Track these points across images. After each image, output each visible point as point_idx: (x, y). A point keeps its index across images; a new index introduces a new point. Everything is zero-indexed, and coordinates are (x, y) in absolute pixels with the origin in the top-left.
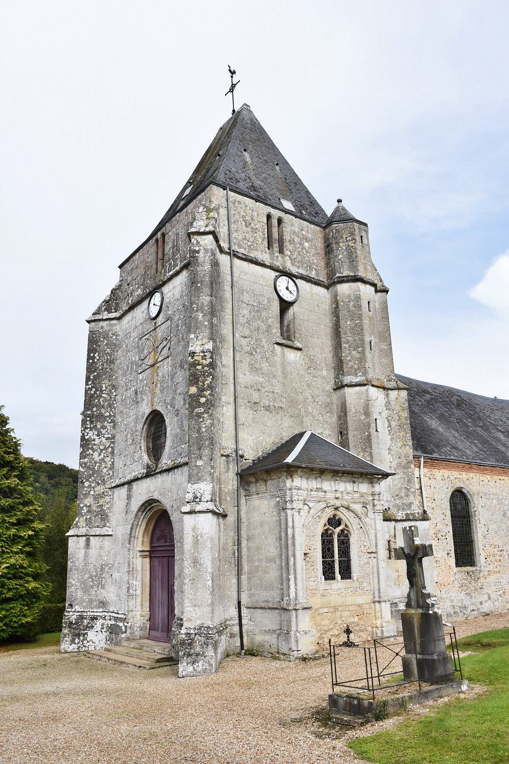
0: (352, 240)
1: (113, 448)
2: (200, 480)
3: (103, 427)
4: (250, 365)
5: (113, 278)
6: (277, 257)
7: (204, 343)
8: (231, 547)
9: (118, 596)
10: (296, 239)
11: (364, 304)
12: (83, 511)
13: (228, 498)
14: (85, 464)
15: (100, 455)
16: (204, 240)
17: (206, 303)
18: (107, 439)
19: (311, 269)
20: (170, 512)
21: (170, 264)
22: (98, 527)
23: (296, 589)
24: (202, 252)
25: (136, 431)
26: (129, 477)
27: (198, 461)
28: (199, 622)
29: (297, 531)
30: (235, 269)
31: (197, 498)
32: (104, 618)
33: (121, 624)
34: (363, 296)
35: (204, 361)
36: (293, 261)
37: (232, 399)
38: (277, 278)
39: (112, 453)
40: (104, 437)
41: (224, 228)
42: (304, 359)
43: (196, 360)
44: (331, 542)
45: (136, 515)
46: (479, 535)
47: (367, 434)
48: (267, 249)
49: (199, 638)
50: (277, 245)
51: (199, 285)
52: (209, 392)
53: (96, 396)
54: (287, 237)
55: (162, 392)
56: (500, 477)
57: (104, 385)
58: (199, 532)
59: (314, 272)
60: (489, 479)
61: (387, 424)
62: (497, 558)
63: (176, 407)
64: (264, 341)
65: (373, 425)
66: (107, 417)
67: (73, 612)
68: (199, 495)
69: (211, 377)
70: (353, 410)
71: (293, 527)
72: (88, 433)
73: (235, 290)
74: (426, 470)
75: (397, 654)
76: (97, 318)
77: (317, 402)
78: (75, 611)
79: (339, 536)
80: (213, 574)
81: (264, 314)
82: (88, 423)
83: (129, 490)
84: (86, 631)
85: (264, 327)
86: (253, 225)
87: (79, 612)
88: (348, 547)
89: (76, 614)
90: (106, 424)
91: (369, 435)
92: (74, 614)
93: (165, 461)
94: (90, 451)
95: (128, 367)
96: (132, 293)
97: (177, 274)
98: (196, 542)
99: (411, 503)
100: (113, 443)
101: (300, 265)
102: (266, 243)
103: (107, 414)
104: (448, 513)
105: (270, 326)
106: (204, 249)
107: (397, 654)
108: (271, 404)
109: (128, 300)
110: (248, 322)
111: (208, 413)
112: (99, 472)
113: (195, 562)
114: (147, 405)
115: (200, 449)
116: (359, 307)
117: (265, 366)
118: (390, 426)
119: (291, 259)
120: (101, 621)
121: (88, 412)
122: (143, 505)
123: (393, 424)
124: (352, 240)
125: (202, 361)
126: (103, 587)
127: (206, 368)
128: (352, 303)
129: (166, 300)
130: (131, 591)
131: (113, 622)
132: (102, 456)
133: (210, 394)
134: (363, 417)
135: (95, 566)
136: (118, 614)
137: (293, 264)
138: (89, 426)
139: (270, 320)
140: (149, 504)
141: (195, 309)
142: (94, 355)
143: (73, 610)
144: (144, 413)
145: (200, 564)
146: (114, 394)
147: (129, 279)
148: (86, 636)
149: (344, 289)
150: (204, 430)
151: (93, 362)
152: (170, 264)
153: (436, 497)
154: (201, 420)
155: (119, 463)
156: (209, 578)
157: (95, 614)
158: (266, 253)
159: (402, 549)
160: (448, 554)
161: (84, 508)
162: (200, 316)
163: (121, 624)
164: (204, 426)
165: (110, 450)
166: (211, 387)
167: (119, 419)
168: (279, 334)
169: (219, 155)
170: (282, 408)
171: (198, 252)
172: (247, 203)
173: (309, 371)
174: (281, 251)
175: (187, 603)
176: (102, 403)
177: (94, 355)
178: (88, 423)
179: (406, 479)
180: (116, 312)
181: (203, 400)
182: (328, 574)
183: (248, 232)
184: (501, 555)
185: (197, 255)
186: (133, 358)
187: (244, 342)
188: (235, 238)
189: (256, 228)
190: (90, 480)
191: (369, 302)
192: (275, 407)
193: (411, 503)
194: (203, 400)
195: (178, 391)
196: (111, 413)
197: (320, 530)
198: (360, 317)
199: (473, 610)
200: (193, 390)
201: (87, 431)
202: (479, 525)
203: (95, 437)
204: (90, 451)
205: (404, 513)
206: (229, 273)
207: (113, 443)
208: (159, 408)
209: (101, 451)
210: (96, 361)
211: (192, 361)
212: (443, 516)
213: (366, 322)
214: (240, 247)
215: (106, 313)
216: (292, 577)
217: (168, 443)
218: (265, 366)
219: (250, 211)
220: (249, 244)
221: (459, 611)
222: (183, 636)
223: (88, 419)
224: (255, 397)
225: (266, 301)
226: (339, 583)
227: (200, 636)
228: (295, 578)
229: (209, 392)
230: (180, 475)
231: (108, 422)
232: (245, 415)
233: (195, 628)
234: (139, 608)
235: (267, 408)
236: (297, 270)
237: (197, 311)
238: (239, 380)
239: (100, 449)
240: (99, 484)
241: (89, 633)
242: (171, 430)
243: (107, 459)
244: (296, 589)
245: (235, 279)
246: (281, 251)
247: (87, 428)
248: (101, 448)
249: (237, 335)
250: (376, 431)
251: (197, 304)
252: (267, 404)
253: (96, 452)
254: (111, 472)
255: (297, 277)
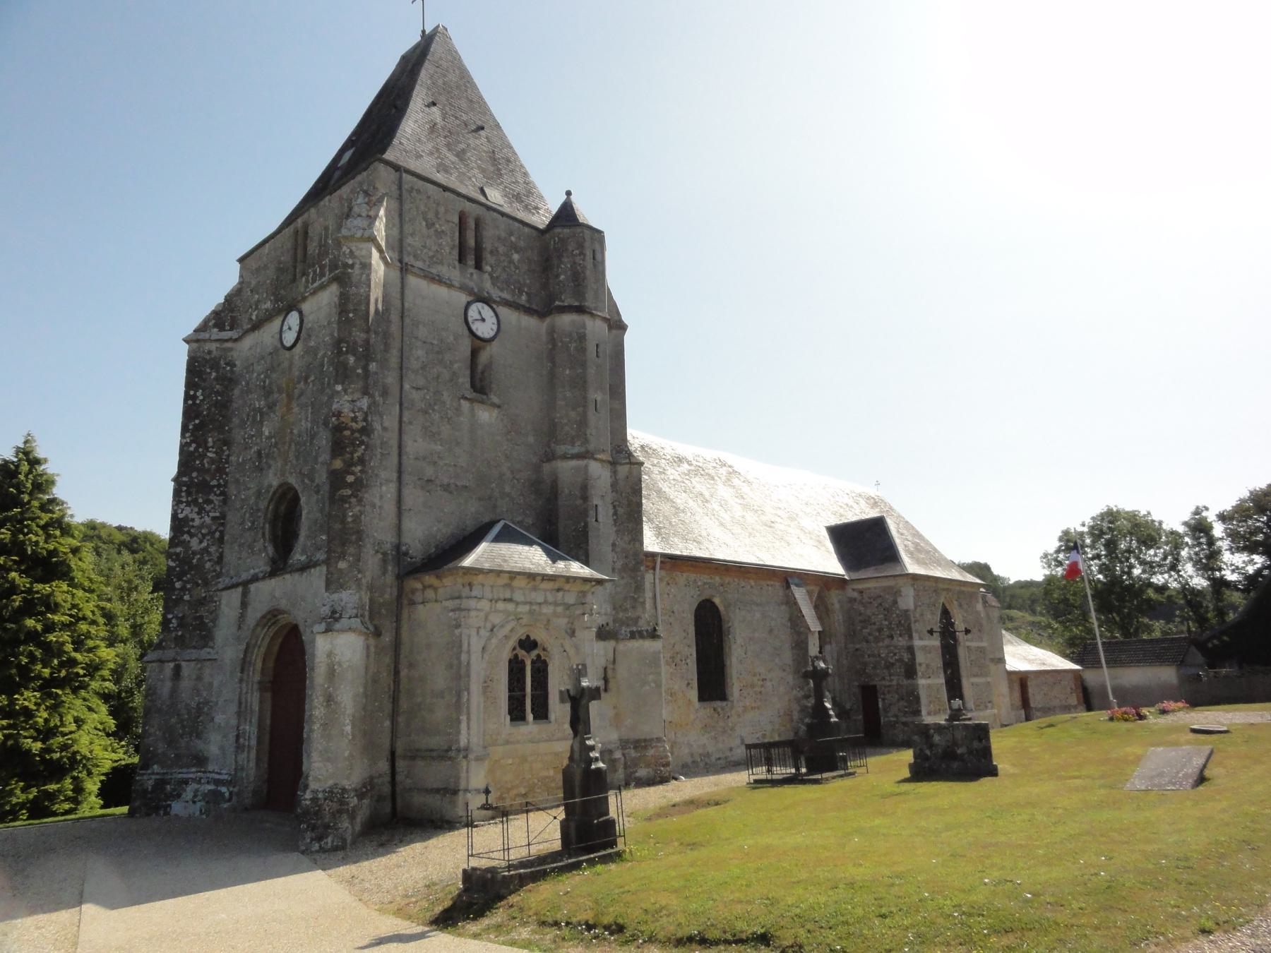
0: (580, 254)
1: (222, 532)
2: (342, 587)
3: (209, 502)
4: (425, 428)
5: (229, 278)
6: (472, 274)
7: (355, 399)
8: (386, 679)
9: (222, 748)
10: (502, 249)
11: (591, 348)
12: (171, 625)
13: (383, 611)
14: (177, 555)
15: (201, 542)
16: (361, 249)
17: (360, 342)
18: (214, 518)
19: (521, 292)
20: (301, 628)
21: (315, 272)
22: (195, 648)
23: (469, 734)
24: (357, 266)
25: (258, 510)
26: (245, 576)
27: (340, 562)
28: (331, 782)
29: (473, 658)
30: (407, 292)
31: (336, 612)
32: (199, 782)
33: (224, 789)
34: (589, 336)
35: (354, 424)
36: (494, 280)
37: (395, 476)
38: (468, 305)
39: (221, 540)
40: (208, 516)
41: (394, 229)
42: (502, 420)
43: (343, 423)
44: (523, 670)
45: (254, 630)
46: (734, 660)
47: (583, 524)
48: (457, 263)
49: (330, 803)
50: (473, 257)
51: (351, 315)
52: (359, 468)
53: (196, 454)
54: (487, 245)
55: (297, 458)
56: (769, 583)
57: (210, 440)
58: (337, 660)
59: (524, 297)
60: (753, 584)
61: (611, 511)
62: (758, 689)
63: (317, 481)
64: (445, 394)
65: (592, 513)
66: (215, 486)
67: (149, 774)
68: (339, 609)
69: (363, 447)
70: (567, 491)
71: (469, 652)
72: (183, 510)
73: (407, 321)
74: (663, 573)
75: (555, 818)
76: (200, 337)
77: (517, 480)
78: (153, 773)
79: (533, 662)
80: (354, 717)
81: (448, 357)
82: (183, 494)
83: (245, 594)
84: (169, 802)
85: (446, 375)
86: (437, 226)
87: (157, 774)
88: (546, 678)
89: (153, 777)
90: (212, 497)
91: (586, 526)
92: (151, 779)
93: (298, 557)
94: (186, 537)
95: (248, 415)
96: (257, 306)
97: (322, 287)
98: (331, 673)
99: (639, 617)
100: (223, 525)
101: (505, 286)
102: (456, 253)
103: (214, 483)
104: (692, 629)
105: (454, 374)
106: (361, 263)
107: (555, 818)
108: (452, 481)
109: (251, 314)
110: (423, 368)
111: (356, 497)
112: (199, 567)
113: (329, 699)
114: (276, 475)
115: (343, 545)
116: (582, 350)
117: (445, 430)
118: (615, 513)
119: (492, 277)
120: (196, 786)
121: (184, 479)
122: (263, 617)
123: (621, 511)
124: (580, 254)
125: (351, 424)
126: (199, 736)
127: (357, 435)
128: (574, 345)
129: (307, 325)
130: (241, 740)
131: (211, 787)
132: (204, 544)
133: (360, 471)
134: (579, 502)
135: (187, 705)
136: (220, 774)
137: (494, 284)
138: (184, 500)
139: (456, 366)
140: (273, 615)
141: (344, 349)
142: (195, 393)
143: (149, 772)
144: (270, 486)
145: (336, 703)
146: (227, 453)
147: (254, 283)
148: (168, 809)
149: (566, 320)
150: (350, 520)
151: (194, 403)
152: (315, 272)
153: (675, 608)
154: (347, 506)
155: (231, 556)
156: (348, 721)
157: (185, 776)
158: (455, 268)
159: (568, 691)
160: (688, 684)
161: (174, 621)
162: (352, 359)
163: (224, 789)
164: (350, 514)
165: (217, 534)
166: (362, 461)
167: (232, 490)
168: (468, 385)
169: (396, 107)
170: (466, 487)
171: (352, 266)
172: (430, 193)
173: (509, 437)
174: (478, 267)
175: (315, 756)
176: (206, 465)
177: (195, 393)
178: (183, 494)
179: (634, 585)
180: (231, 329)
181: (350, 479)
182: (517, 714)
183: (429, 237)
184: (762, 686)
185: (350, 270)
186: (257, 403)
187: (416, 395)
188: (409, 245)
189: (443, 231)
190: (185, 578)
191: (597, 345)
192: (456, 486)
193: (639, 617)
194: (350, 479)
195: (320, 460)
196: (221, 481)
197: (506, 655)
198: (583, 365)
199: (719, 759)
200: (338, 464)
201: (182, 506)
202: (734, 647)
203: (194, 516)
204: (186, 537)
205: (628, 630)
206: (398, 296)
207: (223, 525)
208: (292, 480)
209: (204, 536)
210: (198, 402)
211: (336, 423)
212: (685, 634)
213: (591, 371)
214: (416, 257)
215: (216, 330)
216: (464, 718)
217: (303, 533)
218: (445, 430)
219: (435, 205)
220: (431, 254)
221: (699, 760)
222: (308, 802)
223: (184, 488)
224: (429, 472)
225: (451, 338)
226: (531, 727)
227: (332, 801)
228: (469, 719)
229: (359, 468)
230: (317, 577)
231: (216, 495)
232: (413, 496)
233: (324, 791)
234: (252, 764)
235: (446, 488)
236: (500, 294)
237: (347, 352)
238: (408, 449)
239: (202, 534)
240: (198, 585)
241: (174, 804)
242: (308, 513)
243: (212, 549)
244: (469, 734)
245: (406, 305)
246: (478, 267)
247: (182, 502)
248: (203, 531)
249: (407, 386)
250: (596, 520)
251: (347, 342)
252: (446, 481)
253: (195, 538)
254: (218, 568)
255: (499, 303)
